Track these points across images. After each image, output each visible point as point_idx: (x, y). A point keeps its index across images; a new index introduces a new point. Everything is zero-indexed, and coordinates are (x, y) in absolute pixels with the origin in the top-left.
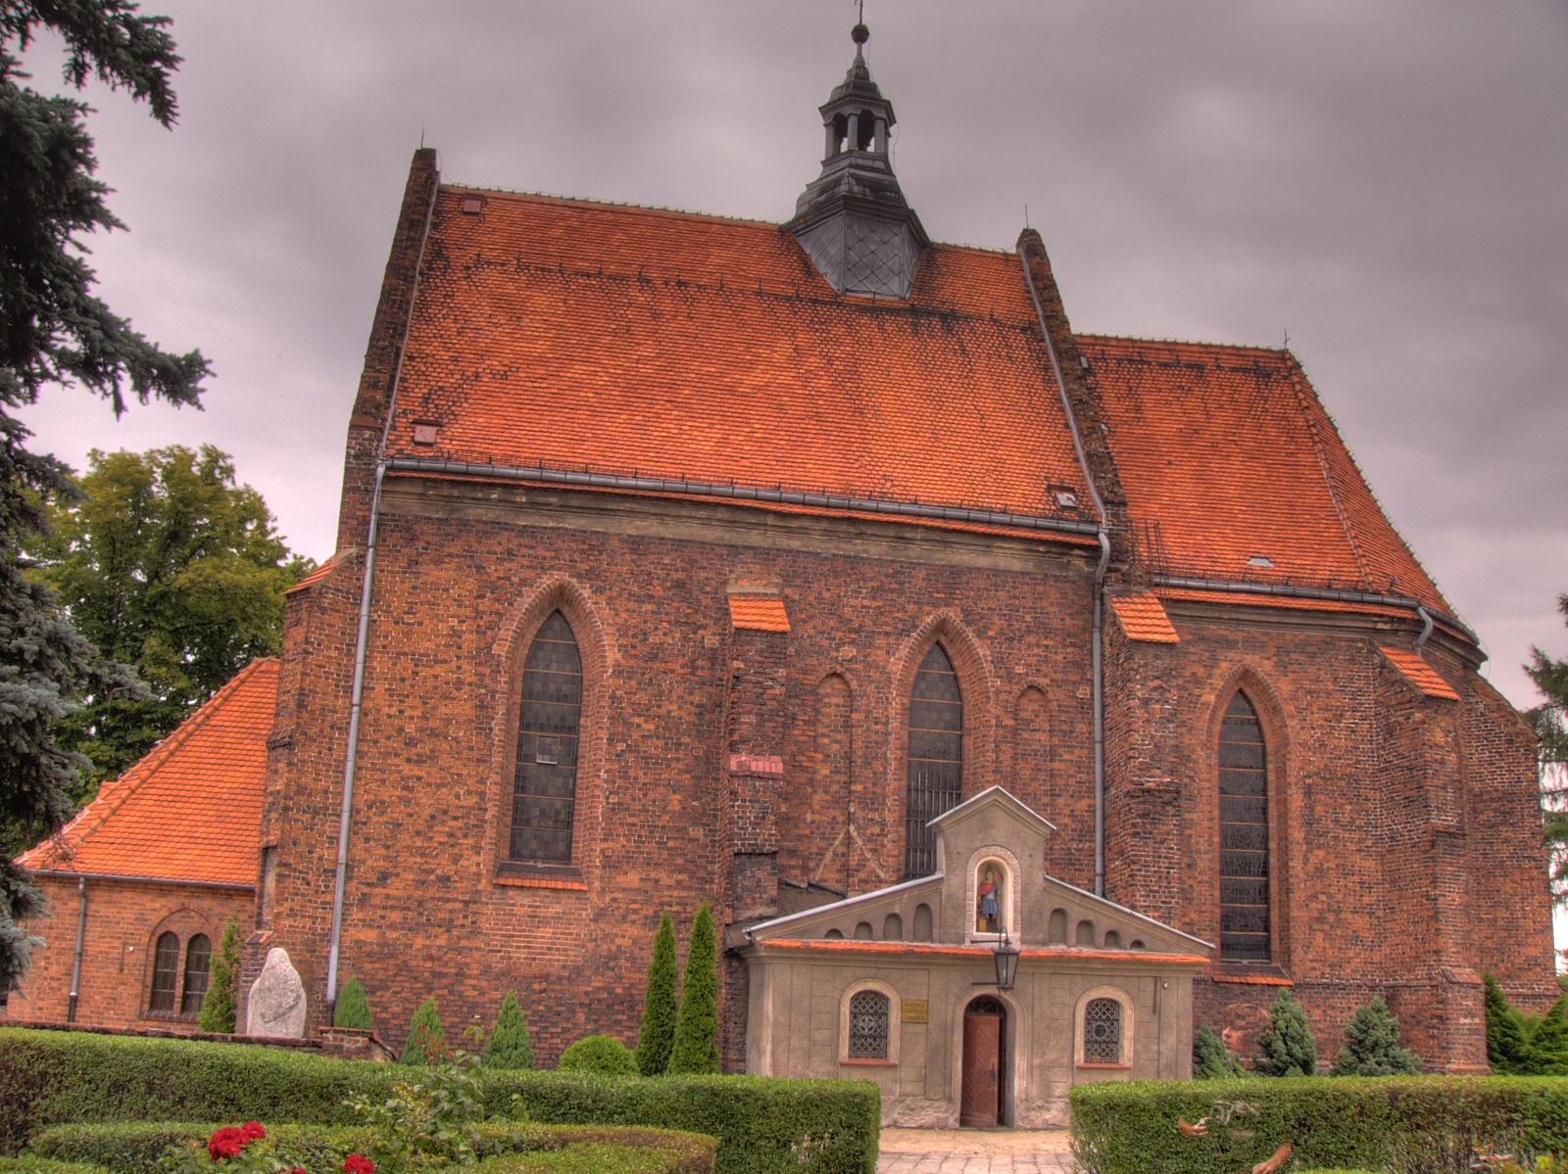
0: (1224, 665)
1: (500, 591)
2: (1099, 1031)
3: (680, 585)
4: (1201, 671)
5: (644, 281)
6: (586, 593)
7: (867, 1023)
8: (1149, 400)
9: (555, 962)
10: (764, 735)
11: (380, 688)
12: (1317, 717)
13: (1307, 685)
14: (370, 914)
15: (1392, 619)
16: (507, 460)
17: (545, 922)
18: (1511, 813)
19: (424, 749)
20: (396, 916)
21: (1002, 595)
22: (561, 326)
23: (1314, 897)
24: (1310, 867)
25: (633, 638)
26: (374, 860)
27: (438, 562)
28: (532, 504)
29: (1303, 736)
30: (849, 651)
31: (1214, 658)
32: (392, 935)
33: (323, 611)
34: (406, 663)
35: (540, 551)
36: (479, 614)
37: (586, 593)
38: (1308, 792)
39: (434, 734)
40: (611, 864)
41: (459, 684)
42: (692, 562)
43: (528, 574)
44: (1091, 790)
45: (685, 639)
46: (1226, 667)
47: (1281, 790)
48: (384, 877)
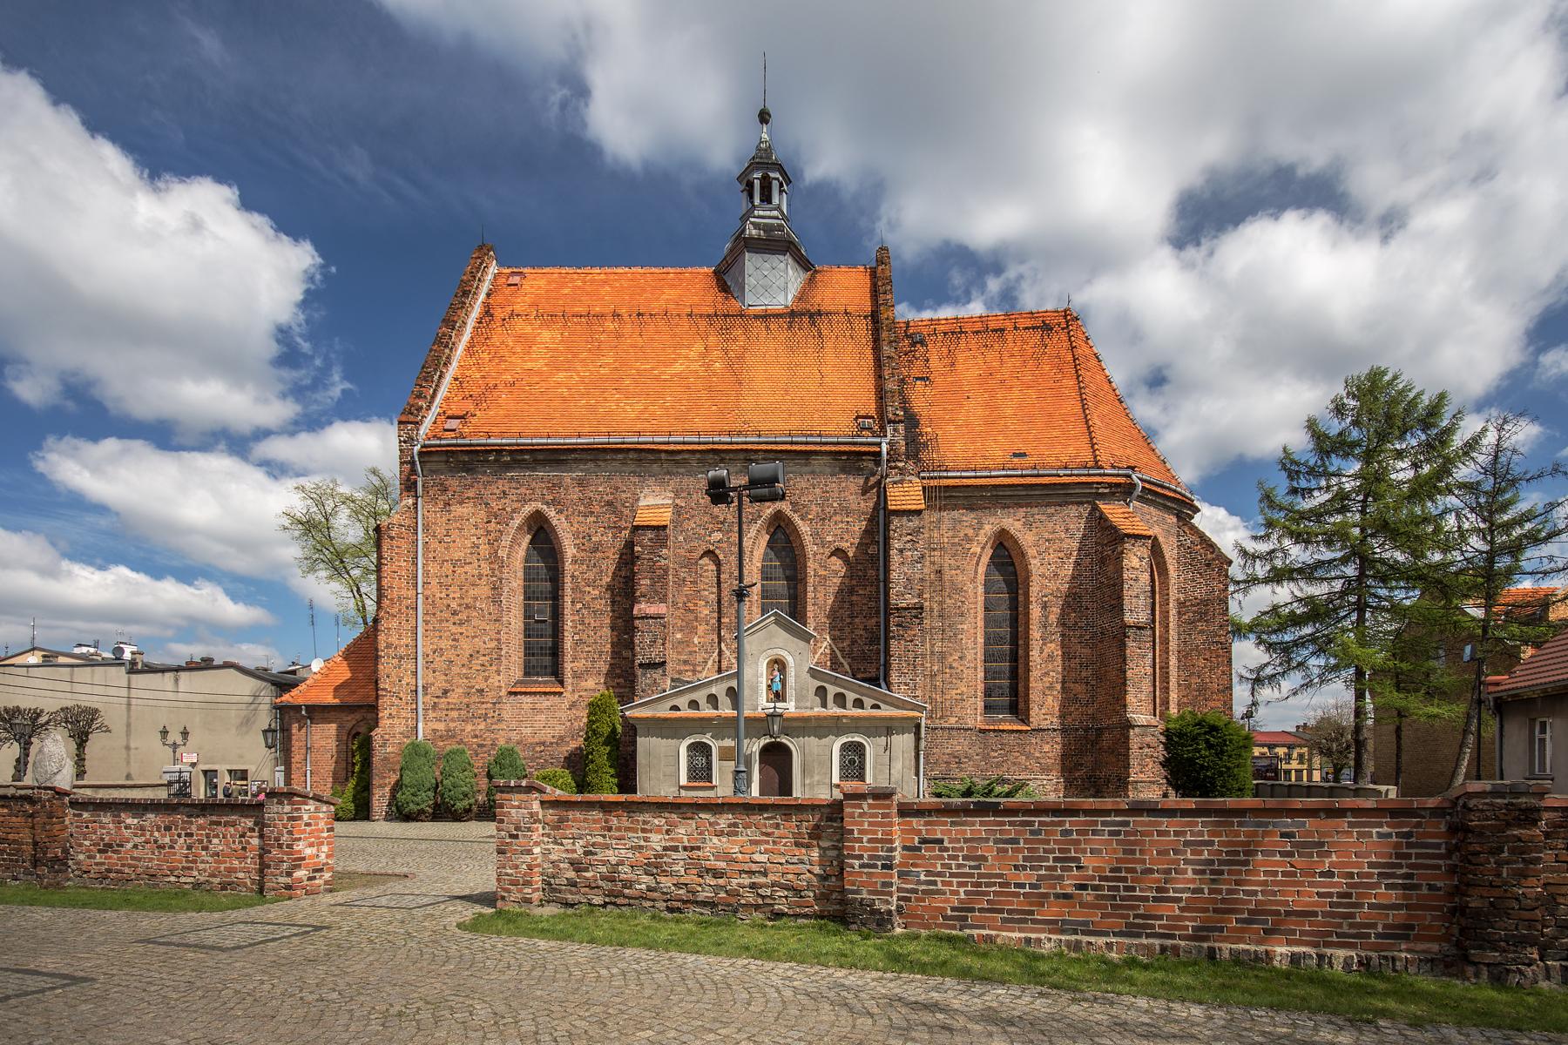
0: (987, 527)
1: (499, 517)
2: (852, 762)
3: (609, 503)
4: (970, 532)
5: (616, 315)
6: (553, 514)
7: (701, 761)
8: (961, 357)
9: (547, 735)
10: (656, 592)
11: (434, 582)
12: (1053, 557)
13: (1046, 535)
14: (439, 714)
15: (1110, 485)
16: (502, 435)
17: (541, 711)
18: (1206, 613)
19: (463, 616)
20: (455, 714)
21: (817, 491)
22: (556, 350)
23: (1047, 674)
24: (1045, 654)
25: (583, 538)
26: (441, 682)
27: (461, 503)
28: (515, 461)
29: (1042, 570)
30: (717, 536)
31: (980, 523)
32: (452, 725)
33: (392, 538)
34: (448, 568)
35: (523, 490)
36: (489, 532)
37: (553, 514)
38: (1045, 606)
39: (468, 607)
40: (577, 676)
41: (480, 576)
42: (617, 488)
43: (515, 505)
44: (878, 612)
45: (614, 537)
46: (989, 528)
47: (1027, 607)
48: (446, 692)
